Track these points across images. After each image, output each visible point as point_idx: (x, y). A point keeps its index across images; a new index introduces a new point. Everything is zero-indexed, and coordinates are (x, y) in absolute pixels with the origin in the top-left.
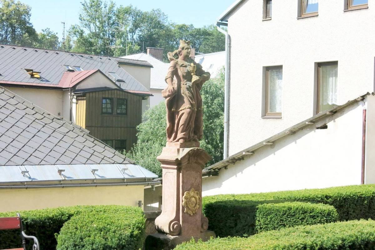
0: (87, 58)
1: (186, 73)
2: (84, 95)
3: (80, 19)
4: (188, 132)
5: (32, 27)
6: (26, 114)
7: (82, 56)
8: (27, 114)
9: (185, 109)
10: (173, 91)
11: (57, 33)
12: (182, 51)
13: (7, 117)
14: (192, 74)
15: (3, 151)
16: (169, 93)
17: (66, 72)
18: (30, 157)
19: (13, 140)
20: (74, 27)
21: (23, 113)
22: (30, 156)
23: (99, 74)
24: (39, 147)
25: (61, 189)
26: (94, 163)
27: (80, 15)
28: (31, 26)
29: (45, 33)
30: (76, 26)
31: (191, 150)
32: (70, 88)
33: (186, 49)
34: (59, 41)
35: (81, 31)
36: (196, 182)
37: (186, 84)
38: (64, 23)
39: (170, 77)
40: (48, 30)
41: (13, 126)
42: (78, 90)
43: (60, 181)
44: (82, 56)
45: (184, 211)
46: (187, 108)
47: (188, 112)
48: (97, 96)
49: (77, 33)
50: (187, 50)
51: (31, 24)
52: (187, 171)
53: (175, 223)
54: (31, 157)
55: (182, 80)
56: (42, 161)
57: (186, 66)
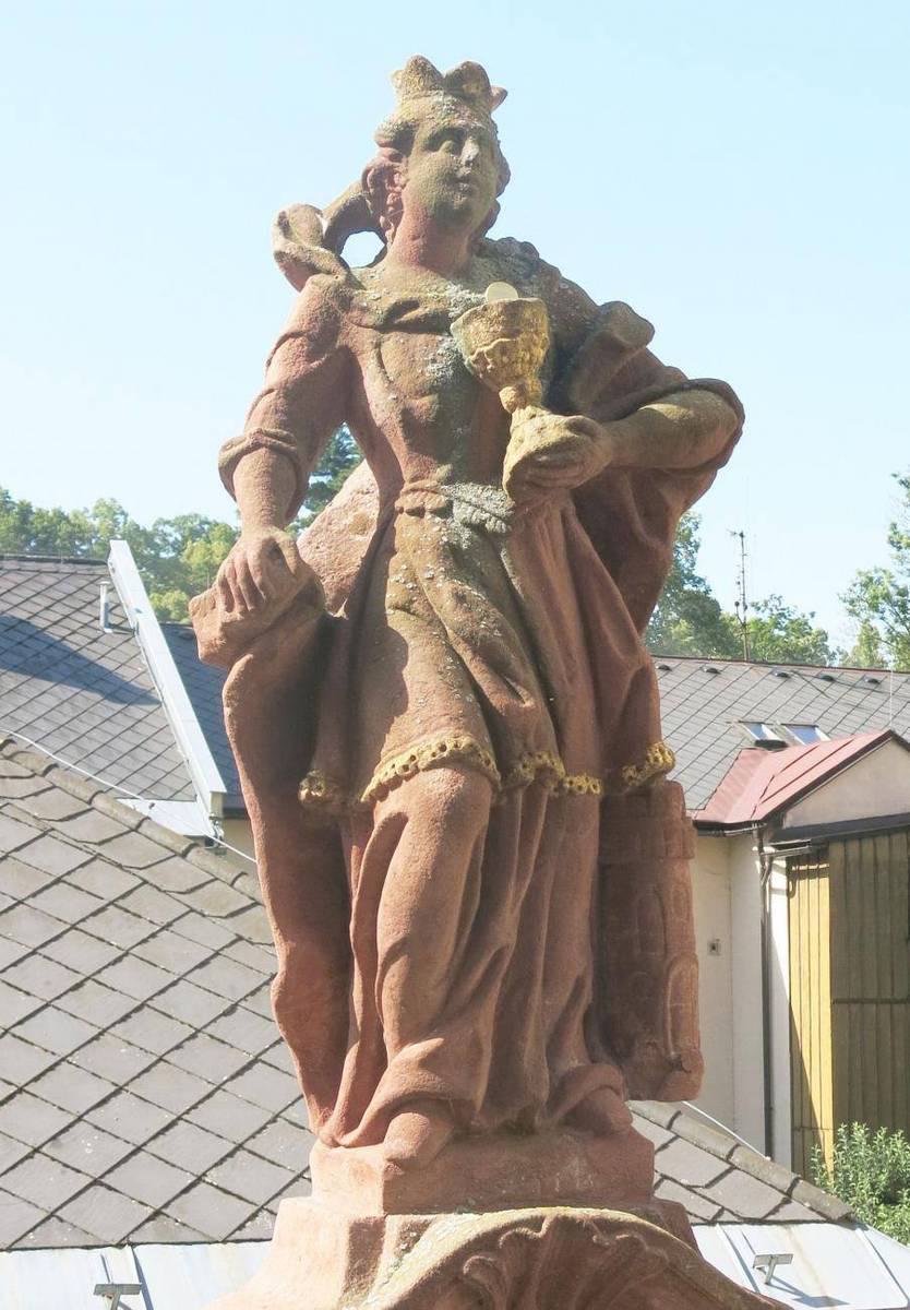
0: (854, 686)
1: (432, 390)
2: (819, 854)
3: (892, 543)
4: (484, 1023)
5: (706, 592)
6: (240, 938)
7: (830, 679)
8: (240, 943)
9: (410, 771)
10: (257, 580)
11: (813, 615)
12: (401, 167)
13: (119, 959)
14: (507, 395)
15: (29, 1157)
16: (230, 608)
17: (744, 753)
18: (186, 1190)
19: (114, 1094)
20: (871, 579)
21: (221, 934)
22: (193, 1185)
23: (891, 751)
24: (259, 1132)
27: (894, 526)
28: (702, 589)
29: (765, 617)
30: (875, 576)
31: (485, 1242)
32: (755, 822)
33: (433, 144)
34: (831, 650)
35: (899, 594)
37: (445, 512)
38: (742, 535)
39: (256, 446)
40: (777, 603)
41: (138, 1009)
42: (792, 828)
44: (830, 679)
46: (426, 758)
47: (439, 810)
48: (883, 854)
49: (884, 605)
50: (440, 155)
51: (701, 580)
54: (194, 1191)
55: (407, 475)
56: (253, 1216)
57: (437, 324)
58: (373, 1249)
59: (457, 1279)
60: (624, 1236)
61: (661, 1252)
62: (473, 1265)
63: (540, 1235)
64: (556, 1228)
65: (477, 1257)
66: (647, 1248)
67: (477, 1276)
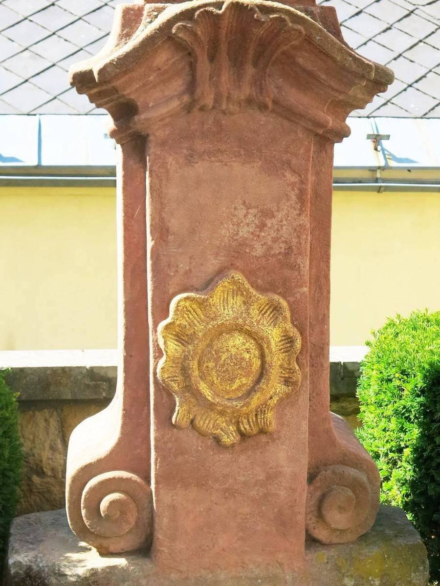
25: (373, 196)
26: (406, 115)
36: (268, 235)
43: (373, 170)
45: (172, 411)
52: (190, 160)
53: (121, 479)
58: (136, 23)
59: (171, 38)
60: (275, 16)
61: (299, 27)
62: (178, 28)
63: (220, 12)
64: (231, 9)
65: (181, 24)
66: (290, 24)
67: (180, 35)
